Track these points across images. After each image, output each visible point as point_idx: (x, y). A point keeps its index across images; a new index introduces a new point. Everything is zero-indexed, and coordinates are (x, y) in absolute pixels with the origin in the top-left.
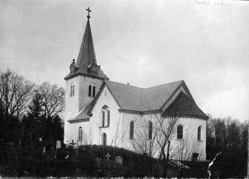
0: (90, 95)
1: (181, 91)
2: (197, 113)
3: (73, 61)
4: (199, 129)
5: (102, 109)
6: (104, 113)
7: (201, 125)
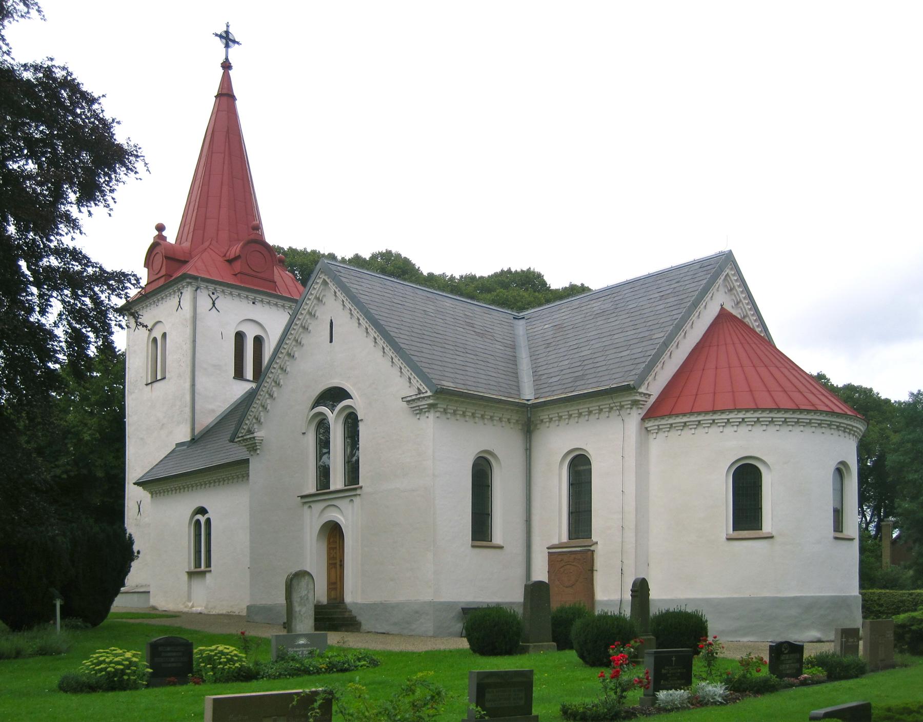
0: (239, 374)
1: (722, 309)
2: (796, 396)
3: (157, 233)
6: (322, 427)
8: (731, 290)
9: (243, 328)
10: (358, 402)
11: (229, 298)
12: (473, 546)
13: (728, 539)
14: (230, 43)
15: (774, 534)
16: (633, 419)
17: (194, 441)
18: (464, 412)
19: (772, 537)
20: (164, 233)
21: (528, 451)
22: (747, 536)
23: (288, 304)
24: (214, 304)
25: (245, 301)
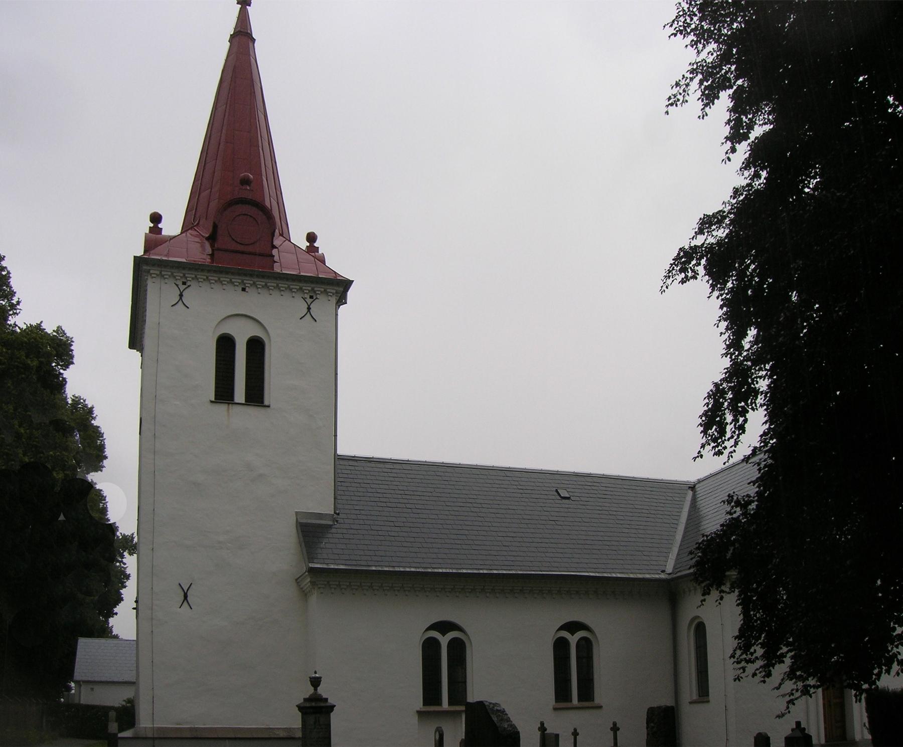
9: (227, 329)
23: (331, 290)
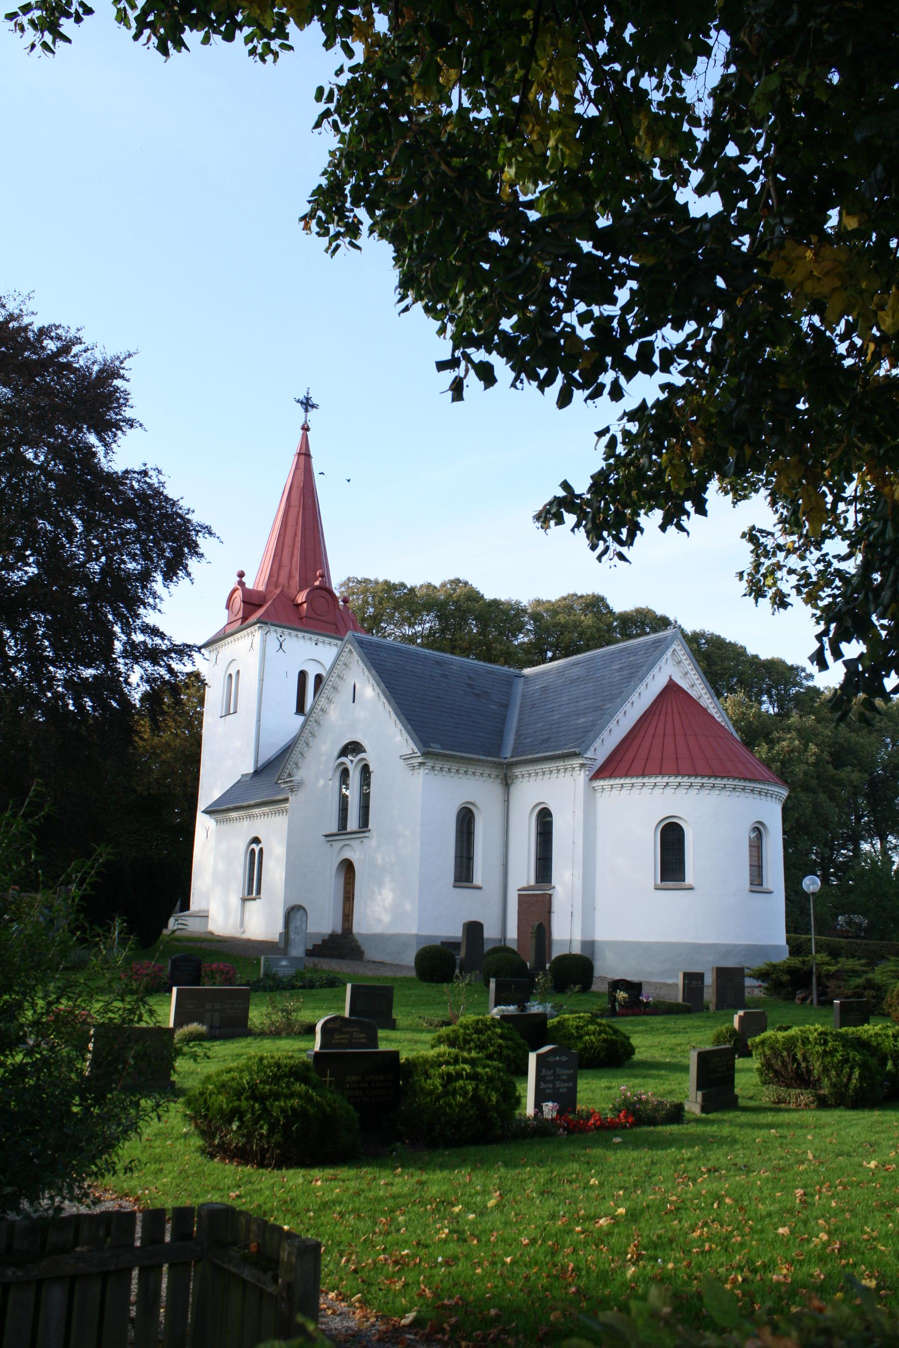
1: (671, 680)
4: (759, 830)
5: (339, 757)
7: (759, 822)
8: (679, 662)
10: (370, 756)
11: (294, 639)
12: (455, 887)
13: (656, 889)
14: (309, 408)
15: (694, 885)
16: (581, 777)
17: (257, 773)
18: (449, 769)
19: (692, 889)
20: (244, 579)
21: (507, 801)
22: (672, 887)
24: (281, 645)
25: (308, 642)
